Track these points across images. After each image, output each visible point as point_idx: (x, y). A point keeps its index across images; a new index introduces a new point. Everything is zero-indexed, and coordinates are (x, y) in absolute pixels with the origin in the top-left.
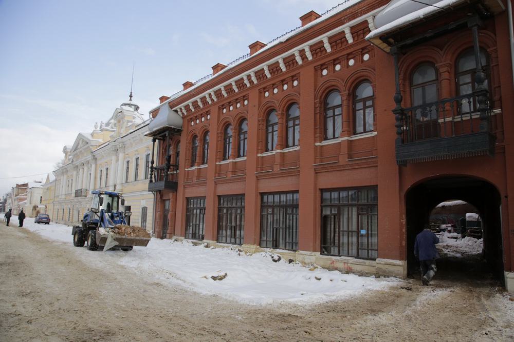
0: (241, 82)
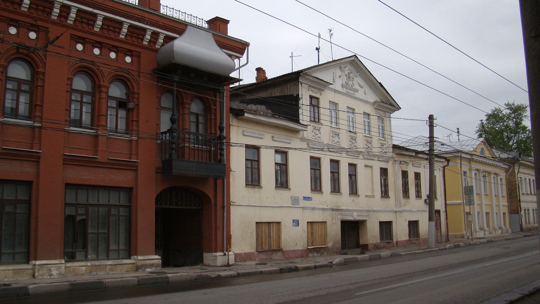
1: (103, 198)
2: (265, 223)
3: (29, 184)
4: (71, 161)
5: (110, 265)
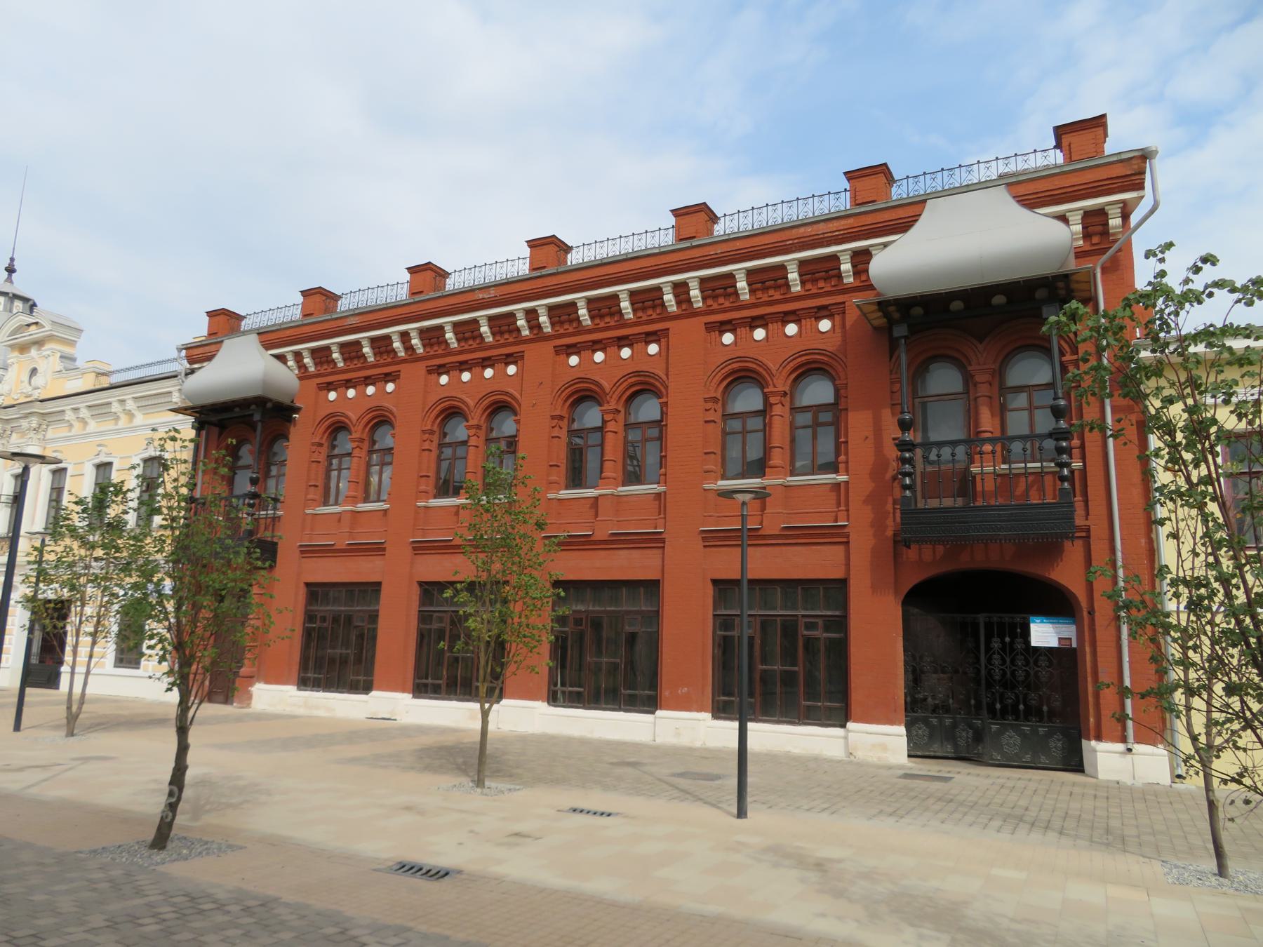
0: (471, 327)
4: (421, 548)
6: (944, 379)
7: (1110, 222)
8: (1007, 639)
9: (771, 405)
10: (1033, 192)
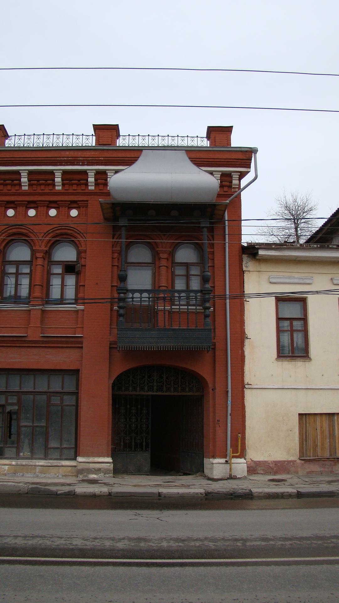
1: (42, 384)
2: (321, 414)
3: (76, 372)
5: (41, 466)
6: (140, 254)
7: (233, 181)
8: (128, 406)
9: (37, 258)
10: (198, 158)
